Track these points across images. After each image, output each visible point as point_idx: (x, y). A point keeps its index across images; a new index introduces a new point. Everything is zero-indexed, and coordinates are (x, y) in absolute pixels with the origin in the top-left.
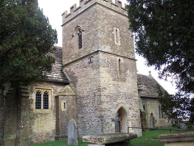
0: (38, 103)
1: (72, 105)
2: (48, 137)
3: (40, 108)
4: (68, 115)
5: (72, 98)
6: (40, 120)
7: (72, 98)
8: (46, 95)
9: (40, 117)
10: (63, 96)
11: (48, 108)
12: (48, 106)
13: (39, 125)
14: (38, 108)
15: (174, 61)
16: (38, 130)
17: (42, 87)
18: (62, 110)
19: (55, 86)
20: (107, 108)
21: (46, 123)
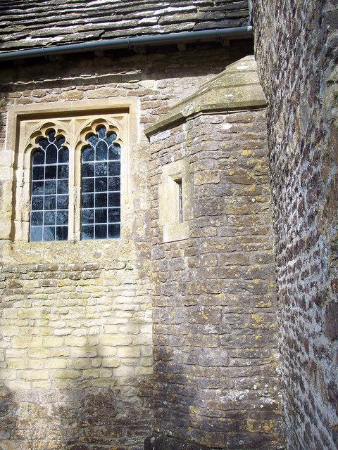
0: (101, 217)
1: (235, 189)
2: (100, 428)
3: (62, 234)
4: (195, 273)
5: (227, 127)
6: (37, 311)
7: (227, 127)
8: (102, 144)
9: (39, 292)
10: (168, 132)
11: (115, 232)
12: (116, 216)
13: (37, 342)
14: (101, 233)
15: (188, 433)
16: (29, 374)
17: (62, 105)
18: (165, 240)
19: (150, 84)
20: (137, 434)
21: (84, 331)
